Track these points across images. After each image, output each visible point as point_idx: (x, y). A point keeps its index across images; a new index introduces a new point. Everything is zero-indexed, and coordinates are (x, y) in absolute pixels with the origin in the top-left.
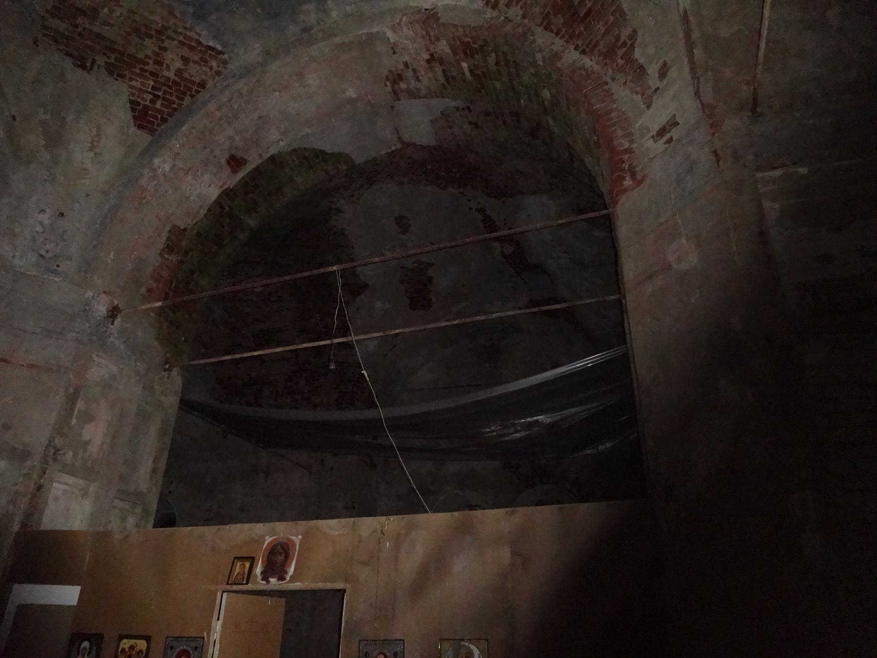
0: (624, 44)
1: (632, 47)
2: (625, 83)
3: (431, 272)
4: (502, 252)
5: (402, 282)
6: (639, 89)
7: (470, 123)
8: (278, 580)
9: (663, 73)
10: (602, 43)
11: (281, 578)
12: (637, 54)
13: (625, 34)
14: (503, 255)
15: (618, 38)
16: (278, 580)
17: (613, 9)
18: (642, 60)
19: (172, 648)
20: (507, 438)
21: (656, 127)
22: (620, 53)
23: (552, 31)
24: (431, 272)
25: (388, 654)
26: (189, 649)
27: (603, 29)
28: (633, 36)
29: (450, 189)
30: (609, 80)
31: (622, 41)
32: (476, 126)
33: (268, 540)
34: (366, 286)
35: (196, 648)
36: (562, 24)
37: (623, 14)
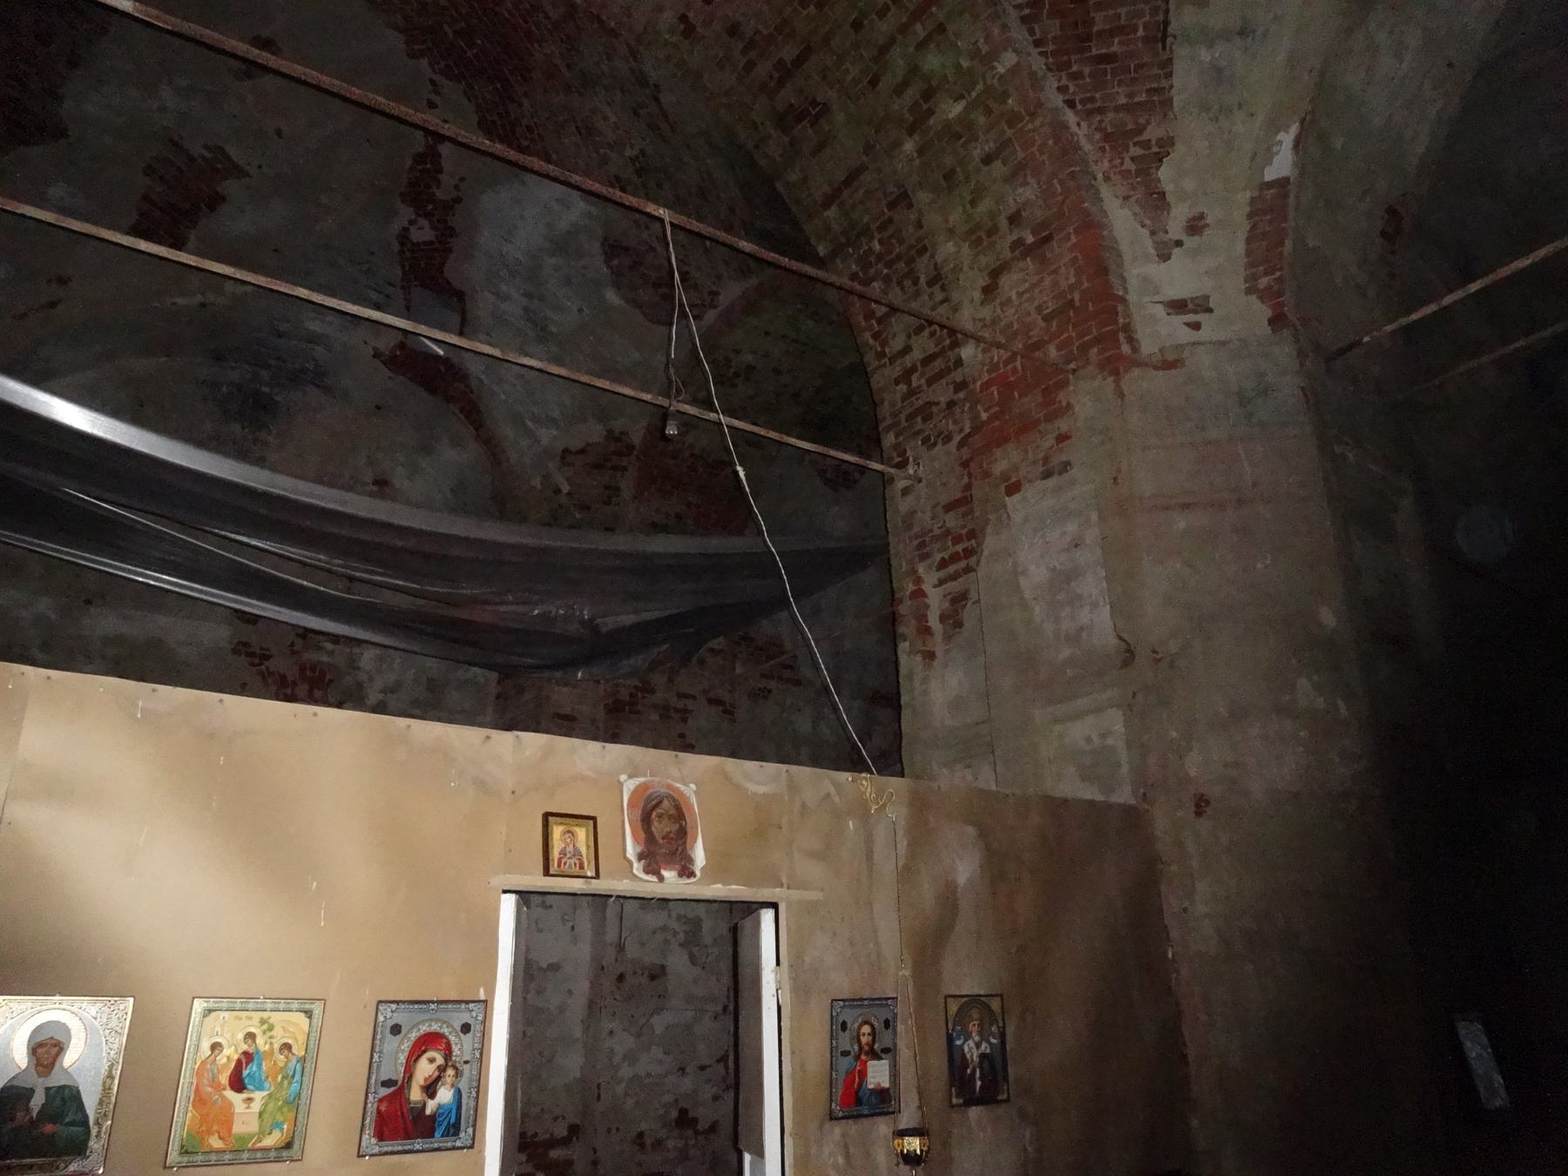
0: (1146, 144)
1: (1159, 159)
2: (1126, 198)
3: (230, 187)
4: (406, 230)
5: (149, 171)
6: (1148, 222)
7: (683, 18)
8: (681, 875)
9: (1195, 226)
10: (1111, 115)
11: (686, 872)
12: (1165, 173)
13: (1153, 133)
14: (404, 236)
15: (1140, 130)
16: (681, 875)
17: (1155, 85)
18: (1169, 188)
19: (396, 1029)
20: (463, 614)
21: (1175, 293)
22: (1136, 151)
23: (1031, 32)
24: (230, 187)
25: (876, 1024)
26: (446, 1031)
27: (1123, 100)
28: (1167, 144)
29: (424, 62)
30: (1100, 176)
31: (1145, 137)
32: (689, 30)
33: (629, 786)
34: (60, 133)
35: (466, 1028)
36: (1055, 38)
37: (1167, 103)
